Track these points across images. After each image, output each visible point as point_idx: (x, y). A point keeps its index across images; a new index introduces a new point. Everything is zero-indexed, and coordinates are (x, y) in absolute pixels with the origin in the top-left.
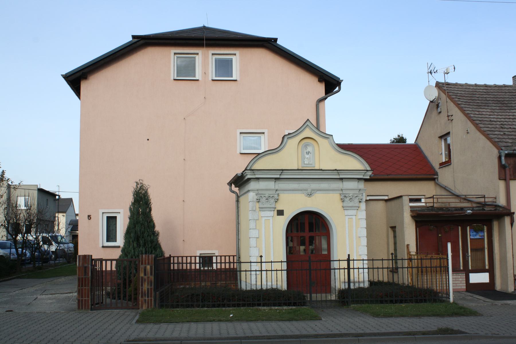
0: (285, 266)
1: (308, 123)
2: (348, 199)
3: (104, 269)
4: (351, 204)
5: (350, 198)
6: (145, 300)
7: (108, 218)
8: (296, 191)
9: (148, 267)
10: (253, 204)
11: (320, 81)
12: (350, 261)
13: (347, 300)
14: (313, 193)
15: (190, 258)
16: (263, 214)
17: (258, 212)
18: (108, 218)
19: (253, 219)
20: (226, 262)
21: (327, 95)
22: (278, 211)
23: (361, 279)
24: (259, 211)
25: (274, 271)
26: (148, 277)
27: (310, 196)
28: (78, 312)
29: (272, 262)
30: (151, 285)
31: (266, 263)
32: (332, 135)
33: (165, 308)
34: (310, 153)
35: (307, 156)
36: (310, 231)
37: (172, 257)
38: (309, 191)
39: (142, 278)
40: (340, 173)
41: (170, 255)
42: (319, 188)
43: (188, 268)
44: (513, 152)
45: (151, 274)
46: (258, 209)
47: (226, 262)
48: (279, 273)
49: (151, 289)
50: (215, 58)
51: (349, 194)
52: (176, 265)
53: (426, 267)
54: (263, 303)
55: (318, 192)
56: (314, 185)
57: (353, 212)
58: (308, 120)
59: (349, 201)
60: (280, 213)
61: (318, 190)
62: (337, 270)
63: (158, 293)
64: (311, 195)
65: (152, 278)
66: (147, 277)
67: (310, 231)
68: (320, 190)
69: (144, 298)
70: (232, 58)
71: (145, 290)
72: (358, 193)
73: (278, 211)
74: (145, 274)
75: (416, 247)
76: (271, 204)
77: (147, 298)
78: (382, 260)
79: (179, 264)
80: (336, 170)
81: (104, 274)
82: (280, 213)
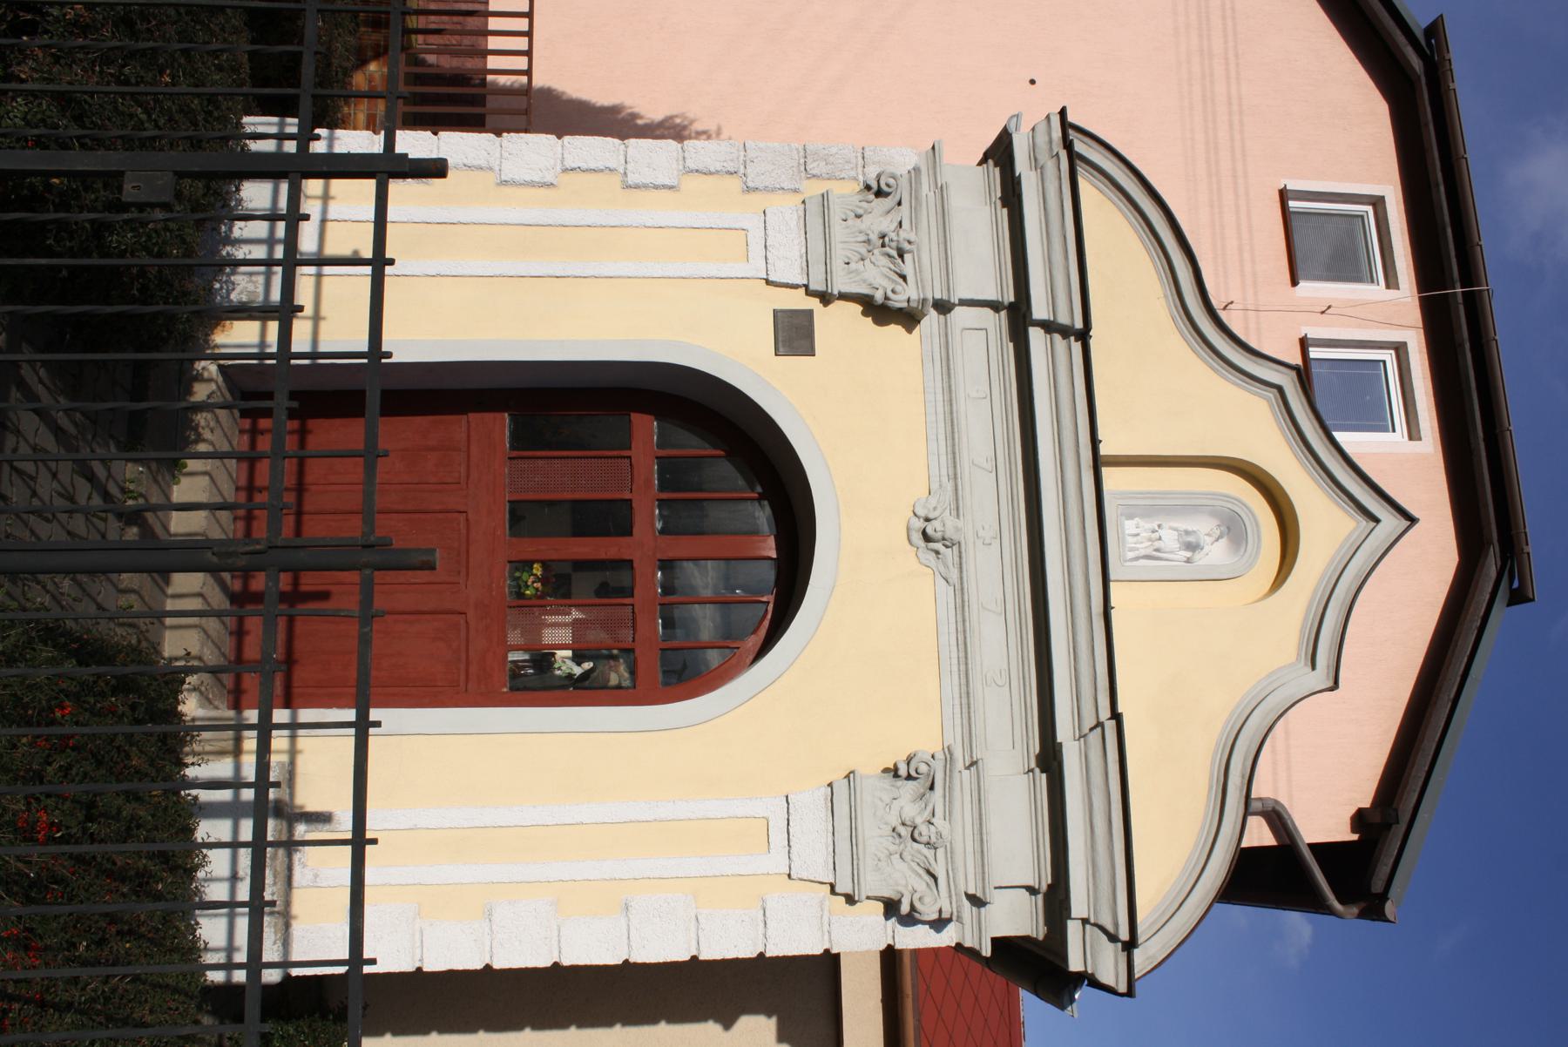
1: (1390, 523)
2: (912, 811)
4: (875, 838)
5: (919, 821)
8: (941, 437)
10: (848, 162)
11: (1360, 820)
14: (937, 553)
16: (785, 211)
19: (750, 154)
21: (1308, 849)
22: (809, 314)
24: (800, 198)
25: (370, 228)
27: (917, 538)
28: (353, 105)
32: (1336, 685)
34: (1188, 561)
35: (1170, 539)
38: (945, 525)
40: (1095, 737)
44: (229, 977)
46: (813, 189)
50: (1384, 362)
51: (949, 815)
55: (946, 593)
57: (814, 858)
58: (1412, 520)
59: (895, 822)
61: (961, 590)
64: (926, 537)
68: (962, 607)
70: (1394, 431)
72: (962, 889)
73: (809, 314)
75: (1490, 614)
76: (853, 265)
81: (472, 22)
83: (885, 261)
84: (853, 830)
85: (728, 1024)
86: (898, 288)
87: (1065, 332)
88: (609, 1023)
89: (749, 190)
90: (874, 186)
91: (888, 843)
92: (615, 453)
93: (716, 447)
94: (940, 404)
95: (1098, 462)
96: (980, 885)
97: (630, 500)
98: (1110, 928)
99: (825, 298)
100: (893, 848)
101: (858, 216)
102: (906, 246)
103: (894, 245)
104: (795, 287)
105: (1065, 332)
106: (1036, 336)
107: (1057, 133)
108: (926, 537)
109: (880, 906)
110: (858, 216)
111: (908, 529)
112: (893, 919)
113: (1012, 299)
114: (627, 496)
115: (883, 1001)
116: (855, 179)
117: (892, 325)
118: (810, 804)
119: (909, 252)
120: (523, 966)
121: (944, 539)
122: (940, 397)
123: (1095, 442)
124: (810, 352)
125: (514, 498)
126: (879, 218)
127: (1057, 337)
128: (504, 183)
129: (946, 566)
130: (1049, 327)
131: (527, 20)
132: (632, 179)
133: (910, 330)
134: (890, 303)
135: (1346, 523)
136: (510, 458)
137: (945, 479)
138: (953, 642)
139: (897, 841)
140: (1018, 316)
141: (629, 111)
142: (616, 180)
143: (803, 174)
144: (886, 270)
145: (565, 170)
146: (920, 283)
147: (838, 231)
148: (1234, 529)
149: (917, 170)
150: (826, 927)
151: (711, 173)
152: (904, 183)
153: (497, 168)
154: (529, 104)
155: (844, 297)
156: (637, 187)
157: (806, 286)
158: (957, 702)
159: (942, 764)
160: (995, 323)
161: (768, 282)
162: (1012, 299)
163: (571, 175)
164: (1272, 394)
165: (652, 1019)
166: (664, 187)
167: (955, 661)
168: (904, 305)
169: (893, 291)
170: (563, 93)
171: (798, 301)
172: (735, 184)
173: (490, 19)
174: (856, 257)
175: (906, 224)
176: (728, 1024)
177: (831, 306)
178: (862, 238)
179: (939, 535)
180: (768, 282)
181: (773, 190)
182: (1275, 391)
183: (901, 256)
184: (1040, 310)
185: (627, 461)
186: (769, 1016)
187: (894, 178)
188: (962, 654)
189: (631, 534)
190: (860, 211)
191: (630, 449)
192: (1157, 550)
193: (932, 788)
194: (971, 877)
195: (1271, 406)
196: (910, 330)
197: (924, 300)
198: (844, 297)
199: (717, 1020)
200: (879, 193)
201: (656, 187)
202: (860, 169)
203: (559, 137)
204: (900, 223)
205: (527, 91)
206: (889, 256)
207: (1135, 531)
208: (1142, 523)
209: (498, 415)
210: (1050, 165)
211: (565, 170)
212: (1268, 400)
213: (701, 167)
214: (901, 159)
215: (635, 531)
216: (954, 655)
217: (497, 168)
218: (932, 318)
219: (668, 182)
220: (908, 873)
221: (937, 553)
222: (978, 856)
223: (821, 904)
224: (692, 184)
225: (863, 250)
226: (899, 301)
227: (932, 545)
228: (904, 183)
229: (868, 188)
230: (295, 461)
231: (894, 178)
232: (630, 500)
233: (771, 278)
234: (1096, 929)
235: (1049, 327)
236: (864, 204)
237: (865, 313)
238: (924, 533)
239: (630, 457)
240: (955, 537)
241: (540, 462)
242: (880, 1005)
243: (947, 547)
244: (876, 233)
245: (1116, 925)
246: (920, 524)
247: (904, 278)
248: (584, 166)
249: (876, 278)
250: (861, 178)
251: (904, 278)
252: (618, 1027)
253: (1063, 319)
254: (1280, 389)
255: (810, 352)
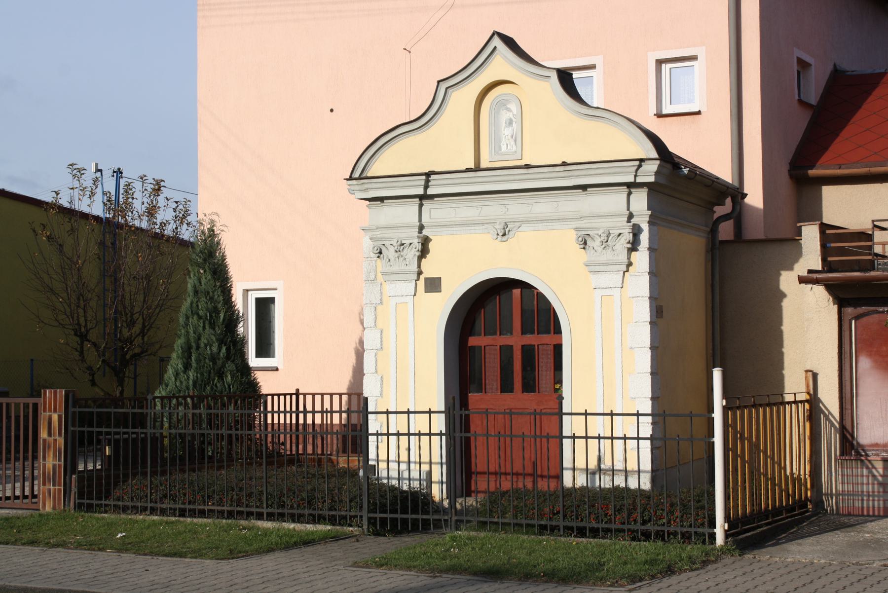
0: (439, 423)
2: (598, 241)
3: (325, 422)
4: (607, 256)
5: (600, 240)
6: (49, 490)
7: (258, 301)
8: (469, 228)
9: (55, 417)
12: (444, 410)
13: (446, 518)
14: (509, 231)
15: (338, 396)
16: (390, 289)
17: (381, 284)
18: (258, 301)
19: (368, 302)
20: (316, 410)
22: (426, 279)
23: (632, 465)
24: (384, 282)
26: (55, 440)
29: (408, 412)
30: (60, 460)
31: (625, 417)
33: (218, 518)
36: (523, 332)
37: (302, 394)
38: (499, 227)
39: (44, 440)
41: (298, 390)
42: (529, 215)
43: (308, 423)
45: (60, 434)
46: (380, 278)
47: (316, 410)
48: (632, 444)
49: (60, 466)
51: (597, 229)
52: (318, 417)
53: (574, 437)
54: (267, 513)
56: (515, 207)
60: (433, 285)
62: (606, 435)
63: (74, 476)
64: (504, 235)
65: (61, 441)
66: (54, 439)
67: (523, 332)
69: (47, 487)
71: (49, 469)
73: (426, 279)
74: (50, 434)
77: (52, 487)
78: (430, 412)
79: (325, 414)
80: (564, 164)
82: (433, 285)
83: (405, 250)
84: (604, 264)
85: (784, 295)
86: (414, 247)
87: (427, 181)
88: (781, 354)
89: (381, 303)
90: (378, 255)
91: (609, 251)
92: (483, 352)
93: (480, 312)
94: (457, 229)
95: (477, 169)
96: (623, 216)
97: (500, 346)
98: (636, 168)
99: (420, 273)
100: (610, 249)
101: (389, 260)
102: (399, 243)
103: (399, 247)
104: (416, 285)
105: (427, 181)
106: (430, 191)
107: (354, 182)
108: (504, 235)
109: (633, 253)
110: (389, 260)
111: (502, 242)
112: (638, 248)
113: (418, 199)
114: (498, 347)
115: (881, 183)
116: (376, 261)
117: (429, 247)
118: (595, 280)
119: (401, 242)
120: (650, 386)
121: (504, 229)
122: (455, 229)
123: (468, 170)
124: (440, 279)
125: (500, 391)
126: (389, 253)
127: (430, 184)
128: (381, 395)
129: (514, 227)
130: (426, 187)
131: (316, 396)
132: (379, 347)
133: (431, 240)
134: (420, 249)
135: (497, 59)
136: (485, 393)
137: (484, 227)
138: (541, 224)
139: (608, 248)
140: (423, 198)
141: (358, 345)
142: (380, 353)
143: (375, 281)
144: (409, 250)
145: (376, 372)
146: (412, 238)
147: (395, 268)
148: (502, 104)
149: (371, 239)
150: (640, 274)
151: (376, 317)
152: (376, 243)
153: (376, 398)
154: (355, 394)
155: (419, 266)
156: (382, 345)
157: (416, 281)
158: (562, 223)
159: (579, 232)
160: (427, 205)
161: (415, 295)
162: (418, 199)
163: (378, 370)
164: (450, 91)
165: (781, 333)
166: (381, 335)
167: (548, 224)
168: (420, 244)
169: (416, 248)
170: (350, 381)
171: (421, 283)
172: (379, 308)
173: (316, 423)
174: (404, 262)
175: (391, 243)
176: (784, 295)
177: (423, 271)
178: (397, 259)
179: (503, 231)
180: (415, 295)
181: (381, 293)
182: (448, 90)
183: (403, 244)
184: (420, 191)
185: (486, 347)
186: (780, 275)
187: (374, 248)
188: (545, 221)
189: (512, 346)
190: (388, 260)
191: (481, 346)
192: (512, 137)
193: (589, 235)
194: (621, 219)
195: (454, 91)
196: (431, 240)
197: (418, 237)
198: (419, 266)
199: (781, 301)
200: (380, 253)
201: (382, 338)
202: (372, 259)
203: (364, 375)
204: (391, 244)
205: (350, 395)
206: (403, 248)
207: (505, 145)
208: (502, 143)
209: (469, 398)
210: (366, 186)
211: (376, 372)
212: (452, 92)
213: (374, 321)
214: (367, 244)
215: (511, 344)
216: (545, 224)
217: (376, 398)
218: (425, 232)
219: (380, 333)
220: (619, 243)
221: (509, 231)
222: (613, 217)
223: (631, 275)
224: (380, 324)
225: (401, 259)
226: (419, 246)
227: (507, 233)
228: (376, 243)
229: (378, 257)
230: (490, 476)
231: (374, 248)
232: (500, 346)
233: (413, 294)
234: (638, 171)
235: (426, 187)
236: (385, 258)
237: (425, 257)
238: (503, 235)
239: (485, 346)
240: (503, 224)
241: (487, 381)
242: (884, 184)
243: (507, 227)
244: (396, 254)
245: (634, 166)
246: (500, 237)
247: (411, 244)
248: (375, 365)
249: (412, 254)
250: (375, 259)
251: (411, 244)
252: (784, 350)
253: (423, 183)
254: (447, 88)
255: (440, 279)
